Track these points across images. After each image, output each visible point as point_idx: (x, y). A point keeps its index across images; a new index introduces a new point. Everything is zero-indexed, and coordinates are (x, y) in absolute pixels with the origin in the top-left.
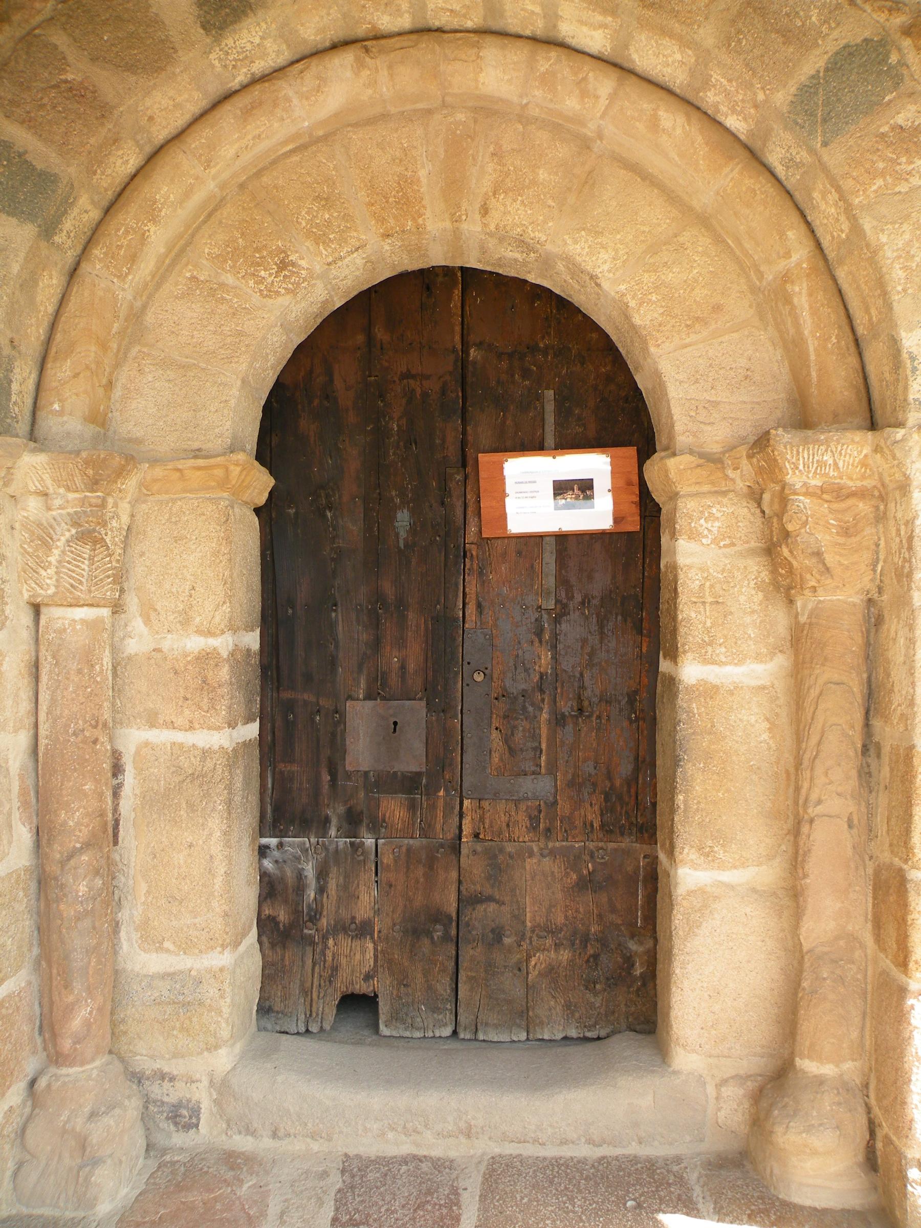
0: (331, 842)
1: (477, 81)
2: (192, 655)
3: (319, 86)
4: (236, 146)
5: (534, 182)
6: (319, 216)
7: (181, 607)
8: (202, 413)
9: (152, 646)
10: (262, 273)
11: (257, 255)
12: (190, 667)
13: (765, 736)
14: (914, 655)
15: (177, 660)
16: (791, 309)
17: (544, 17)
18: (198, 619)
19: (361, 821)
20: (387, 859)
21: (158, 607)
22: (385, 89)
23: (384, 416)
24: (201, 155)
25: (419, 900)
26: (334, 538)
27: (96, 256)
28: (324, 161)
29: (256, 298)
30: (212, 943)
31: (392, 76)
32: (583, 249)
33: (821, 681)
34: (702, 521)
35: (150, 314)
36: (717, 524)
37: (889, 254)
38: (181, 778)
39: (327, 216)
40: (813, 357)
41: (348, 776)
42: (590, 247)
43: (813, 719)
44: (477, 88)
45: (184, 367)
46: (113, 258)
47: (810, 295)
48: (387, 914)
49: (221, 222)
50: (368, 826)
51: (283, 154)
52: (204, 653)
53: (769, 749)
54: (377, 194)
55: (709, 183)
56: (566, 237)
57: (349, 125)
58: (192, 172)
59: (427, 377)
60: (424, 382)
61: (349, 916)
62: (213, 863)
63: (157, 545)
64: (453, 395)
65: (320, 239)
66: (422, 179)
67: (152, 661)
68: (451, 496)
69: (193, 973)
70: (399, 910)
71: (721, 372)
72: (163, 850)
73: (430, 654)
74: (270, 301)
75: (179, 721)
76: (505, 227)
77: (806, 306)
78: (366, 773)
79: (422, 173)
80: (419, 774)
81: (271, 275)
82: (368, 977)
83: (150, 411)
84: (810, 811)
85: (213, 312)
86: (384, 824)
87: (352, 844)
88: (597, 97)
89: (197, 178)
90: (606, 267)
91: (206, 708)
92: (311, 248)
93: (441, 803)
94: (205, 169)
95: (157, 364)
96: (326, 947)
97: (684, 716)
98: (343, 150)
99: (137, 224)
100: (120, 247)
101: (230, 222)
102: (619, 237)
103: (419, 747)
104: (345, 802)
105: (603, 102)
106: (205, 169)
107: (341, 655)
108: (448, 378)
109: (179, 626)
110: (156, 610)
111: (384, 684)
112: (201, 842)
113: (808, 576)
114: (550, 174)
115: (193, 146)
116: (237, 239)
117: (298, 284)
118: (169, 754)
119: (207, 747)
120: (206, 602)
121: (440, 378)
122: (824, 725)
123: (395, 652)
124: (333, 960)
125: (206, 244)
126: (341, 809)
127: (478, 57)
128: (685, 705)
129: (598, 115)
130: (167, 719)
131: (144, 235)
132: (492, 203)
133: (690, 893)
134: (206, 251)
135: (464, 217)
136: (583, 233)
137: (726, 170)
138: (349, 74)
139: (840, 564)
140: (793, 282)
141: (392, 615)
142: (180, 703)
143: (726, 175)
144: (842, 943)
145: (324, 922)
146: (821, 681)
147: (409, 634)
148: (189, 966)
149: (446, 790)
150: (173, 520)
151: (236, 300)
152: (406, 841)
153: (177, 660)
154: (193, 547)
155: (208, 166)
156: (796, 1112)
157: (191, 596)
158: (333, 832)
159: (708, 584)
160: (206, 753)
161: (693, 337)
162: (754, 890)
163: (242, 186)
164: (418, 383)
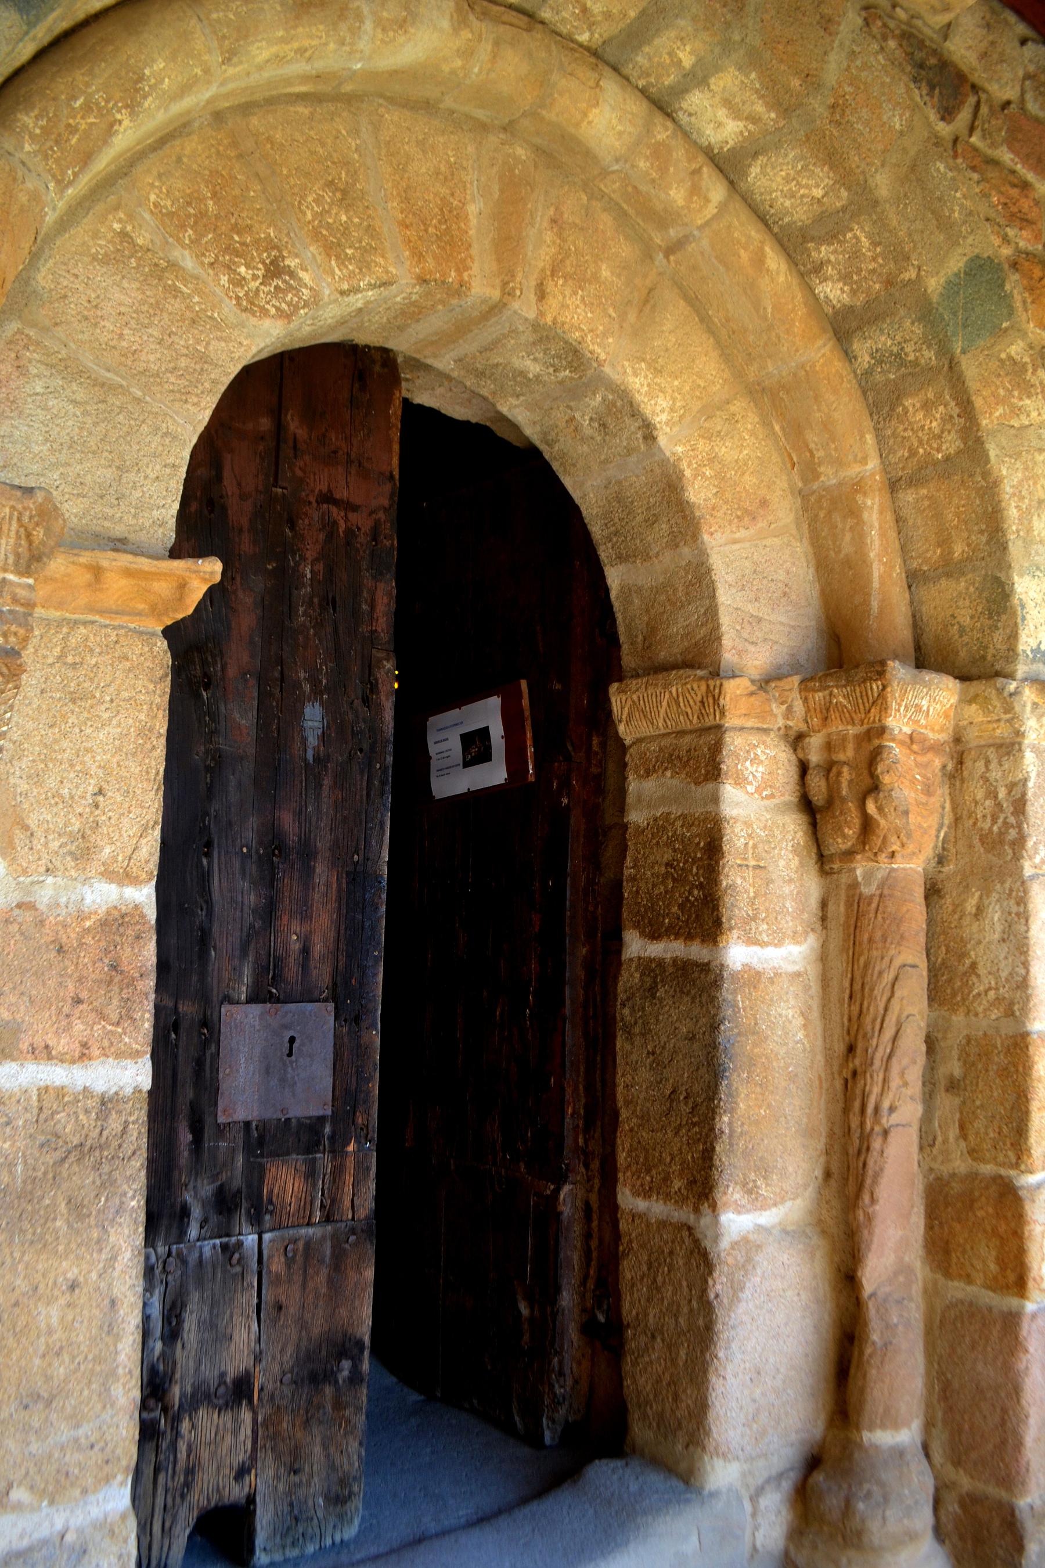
0: (191, 1249)
1: (585, 115)
2: (94, 918)
3: (405, 21)
4: (274, 49)
5: (596, 278)
6: (334, 212)
7: (76, 825)
8: (132, 476)
9: (15, 897)
10: (242, 270)
11: (237, 238)
12: (89, 940)
13: (800, 1035)
14: (1027, 931)
15: (65, 926)
16: (857, 524)
17: (685, 76)
18: (107, 850)
19: (238, 1206)
20: (277, 1265)
21: (32, 822)
22: (476, 70)
23: (294, 554)
24: (224, 37)
25: (318, 1326)
26: (212, 732)
27: (25, 126)
28: (344, 132)
29: (228, 309)
30: (107, 1469)
31: (494, 57)
32: (642, 385)
33: (897, 963)
34: (748, 764)
35: (43, 271)
36: (761, 769)
37: (1008, 489)
38: (58, 1155)
39: (344, 218)
40: (876, 584)
41: (221, 1130)
42: (649, 385)
43: (886, 1009)
44: (578, 125)
45: (103, 385)
46: (57, 142)
47: (881, 513)
48: (274, 1358)
49: (179, 160)
50: (248, 1212)
51: (286, 95)
52: (116, 913)
53: (804, 1050)
54: (414, 214)
55: (797, 350)
56: (626, 364)
57: (381, 96)
58: (206, 57)
59: (353, 508)
60: (350, 515)
61: (216, 1373)
62: (117, 1312)
63: (36, 702)
64: (388, 543)
65: (332, 249)
66: (471, 217)
67: (15, 927)
68: (378, 693)
69: (70, 1538)
70: (290, 1350)
71: (765, 582)
72: (16, 1304)
73: (343, 927)
74: (253, 321)
75: (62, 1044)
76: (563, 324)
77: (876, 525)
78: (247, 1124)
79: (472, 209)
80: (321, 1119)
81: (255, 277)
82: (241, 1473)
83: (36, 449)
84: (884, 1121)
85: (158, 306)
86: (271, 1208)
87: (225, 1247)
88: (708, 201)
89: (207, 71)
90: (664, 417)
91: (114, 1017)
92: (319, 258)
93: (350, 1164)
94: (223, 63)
95: (52, 366)
96: (177, 1435)
97: (730, 1012)
98: (370, 127)
99: (107, 101)
100: (72, 130)
101: (195, 167)
102: (676, 383)
103: (324, 1080)
104: (214, 1178)
105: (711, 210)
106: (223, 63)
107: (215, 929)
108: (381, 515)
109: (69, 862)
110: (26, 828)
111: (276, 980)
112: (94, 1276)
113: (894, 839)
114: (612, 273)
115: (214, 16)
116: (205, 198)
117: (297, 308)
118: (35, 1111)
119: (112, 1092)
120: (125, 821)
121: (370, 514)
122: (899, 1017)
123: (295, 926)
124: (188, 1456)
125: (152, 185)
126: (207, 1189)
127: (597, 85)
128: (730, 997)
129: (699, 222)
130: (38, 1041)
131: (112, 126)
132: (550, 286)
133: (734, 1245)
134: (153, 197)
135: (518, 293)
136: (643, 365)
137: (820, 343)
138: (445, 24)
139: (920, 826)
140: (865, 494)
141: (292, 867)
142: (66, 1010)
143: (819, 349)
144: (901, 1279)
145: (176, 1392)
146: (897, 963)
147: (316, 896)
148: (59, 1526)
149: (358, 1142)
150: (70, 659)
151: (196, 299)
152: (303, 1231)
153: (65, 926)
154: (106, 715)
155: (229, 59)
156: (886, 1499)
157: (97, 806)
158: (193, 1232)
159: (751, 843)
160: (107, 1103)
161: (742, 533)
162: (785, 1232)
163: (218, 117)
164: (342, 514)
